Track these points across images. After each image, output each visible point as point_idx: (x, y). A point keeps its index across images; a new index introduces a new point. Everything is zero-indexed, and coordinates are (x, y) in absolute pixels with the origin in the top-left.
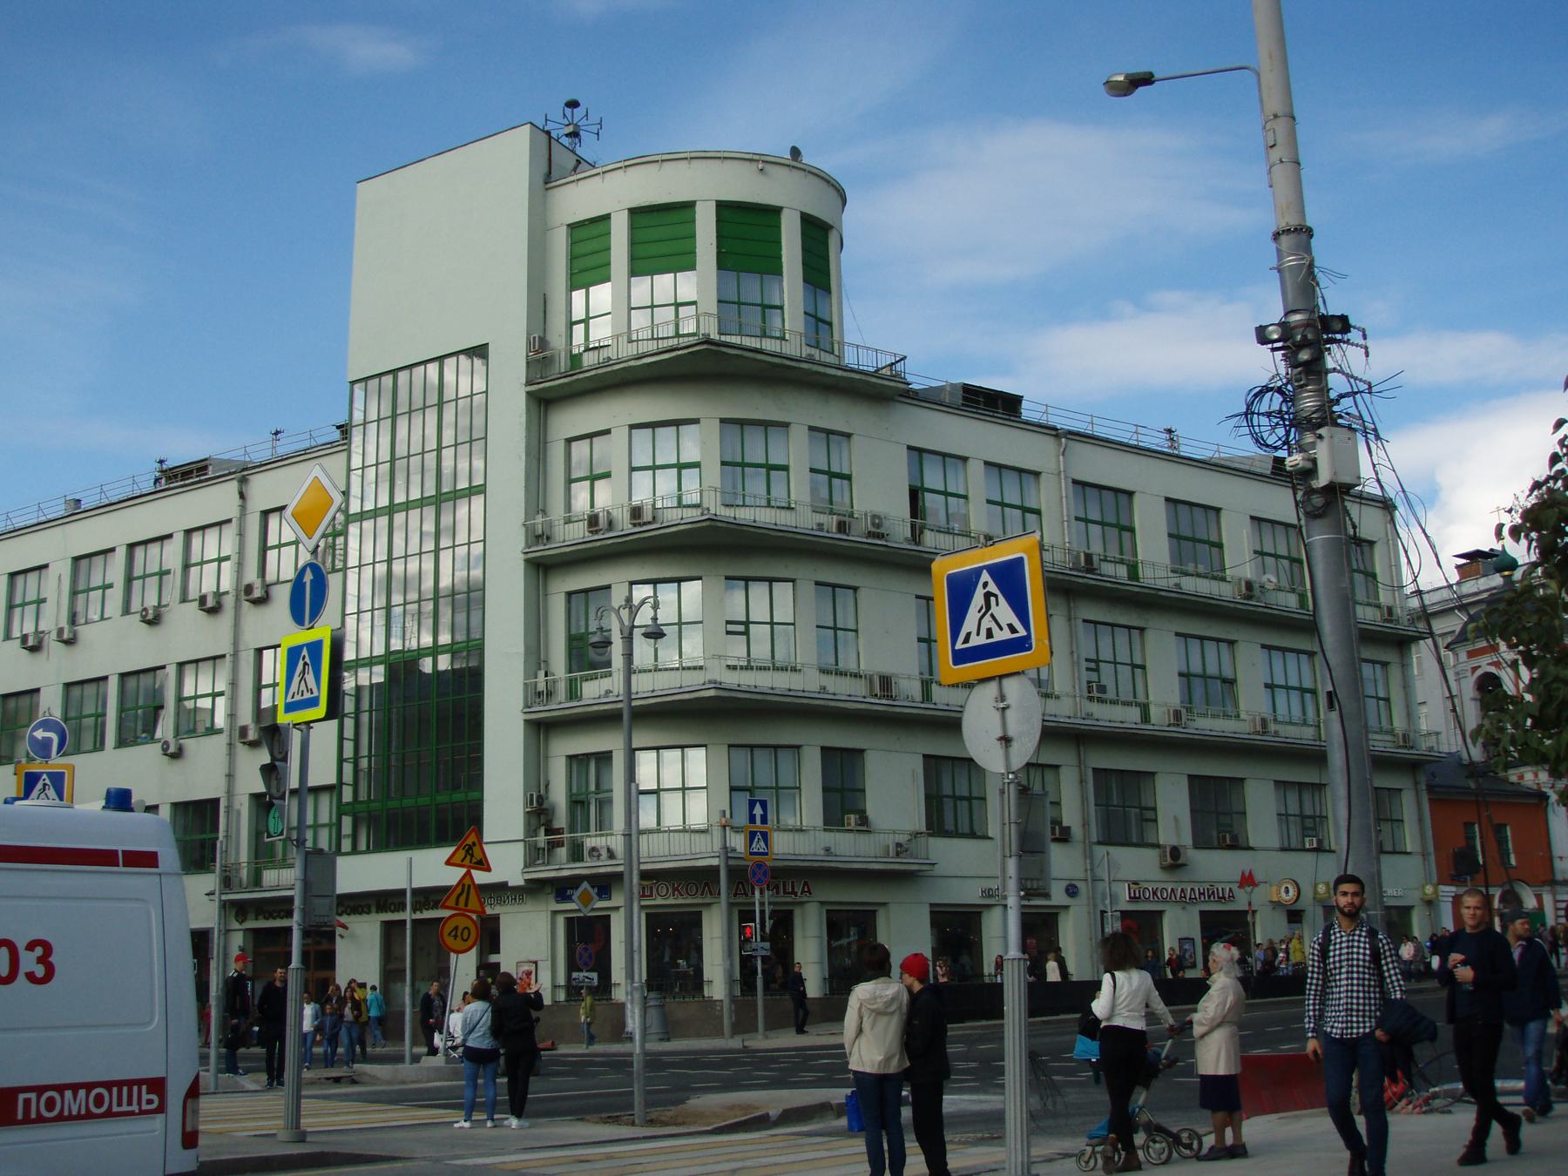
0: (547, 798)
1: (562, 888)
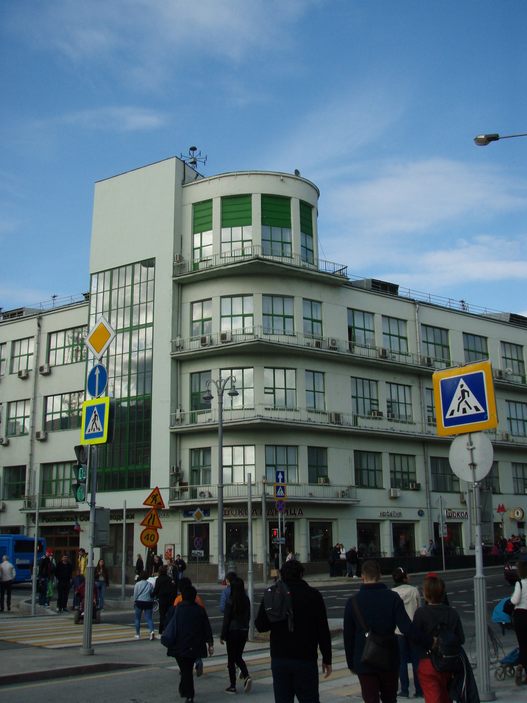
0: (180, 468)
1: (187, 511)
